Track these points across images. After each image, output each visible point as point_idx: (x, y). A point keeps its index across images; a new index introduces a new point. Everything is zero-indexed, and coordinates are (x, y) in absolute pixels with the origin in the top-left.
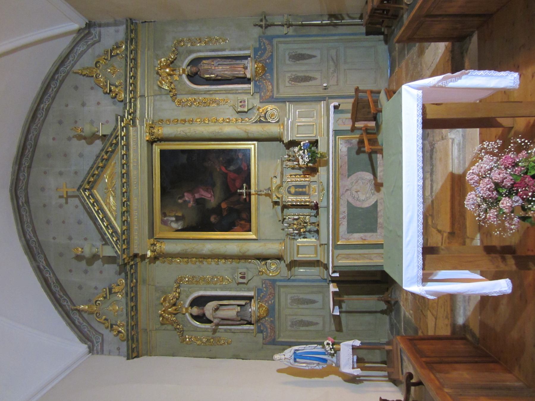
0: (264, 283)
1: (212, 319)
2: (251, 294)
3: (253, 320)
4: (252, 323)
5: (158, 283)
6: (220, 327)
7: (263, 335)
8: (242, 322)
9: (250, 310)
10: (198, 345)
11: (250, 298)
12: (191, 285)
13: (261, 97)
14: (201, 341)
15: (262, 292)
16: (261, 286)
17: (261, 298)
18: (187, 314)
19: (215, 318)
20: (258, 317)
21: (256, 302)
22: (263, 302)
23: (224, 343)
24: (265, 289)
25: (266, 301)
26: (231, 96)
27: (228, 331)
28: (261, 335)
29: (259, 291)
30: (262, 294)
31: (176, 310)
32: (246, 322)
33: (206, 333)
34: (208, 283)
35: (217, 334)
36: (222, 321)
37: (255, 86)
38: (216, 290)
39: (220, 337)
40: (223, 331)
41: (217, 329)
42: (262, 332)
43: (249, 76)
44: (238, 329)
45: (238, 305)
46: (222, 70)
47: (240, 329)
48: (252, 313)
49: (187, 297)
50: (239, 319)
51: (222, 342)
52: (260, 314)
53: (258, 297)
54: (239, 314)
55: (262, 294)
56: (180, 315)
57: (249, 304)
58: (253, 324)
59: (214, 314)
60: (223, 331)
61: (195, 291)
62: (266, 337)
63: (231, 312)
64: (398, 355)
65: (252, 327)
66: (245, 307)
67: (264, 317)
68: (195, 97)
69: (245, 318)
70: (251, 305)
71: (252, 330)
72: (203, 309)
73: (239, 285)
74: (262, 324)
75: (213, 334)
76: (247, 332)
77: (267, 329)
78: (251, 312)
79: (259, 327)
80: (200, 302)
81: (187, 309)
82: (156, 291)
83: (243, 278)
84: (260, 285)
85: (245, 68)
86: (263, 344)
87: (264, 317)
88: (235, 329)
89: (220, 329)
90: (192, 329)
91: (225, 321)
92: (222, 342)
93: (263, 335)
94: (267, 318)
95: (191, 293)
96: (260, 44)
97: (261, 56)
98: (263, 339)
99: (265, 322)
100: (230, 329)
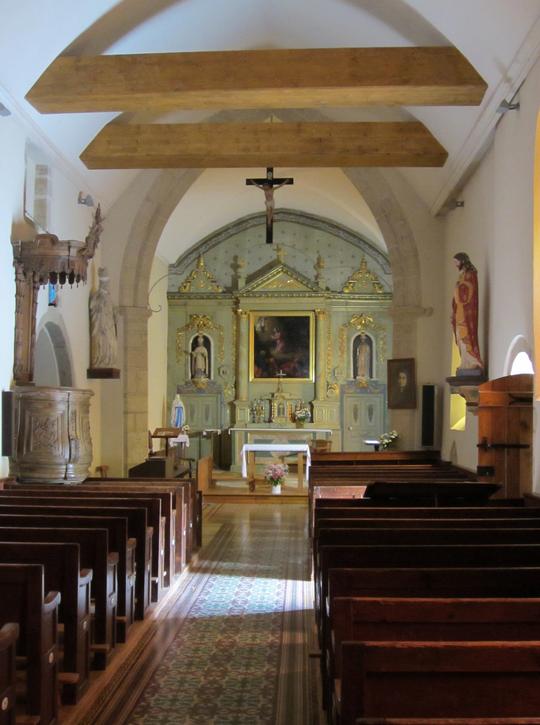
2: (212, 377)
3: (196, 380)
11: (209, 377)
13: (344, 385)
26: (346, 365)
29: (214, 383)
35: (184, 354)
37: (352, 382)
43: (358, 377)
45: (205, 370)
46: (363, 359)
49: (210, 334)
63: (201, 364)
67: (196, 386)
68: (345, 340)
76: (186, 374)
85: (363, 375)
91: (194, 361)
96: (380, 385)
97: (372, 385)
100: (188, 363)
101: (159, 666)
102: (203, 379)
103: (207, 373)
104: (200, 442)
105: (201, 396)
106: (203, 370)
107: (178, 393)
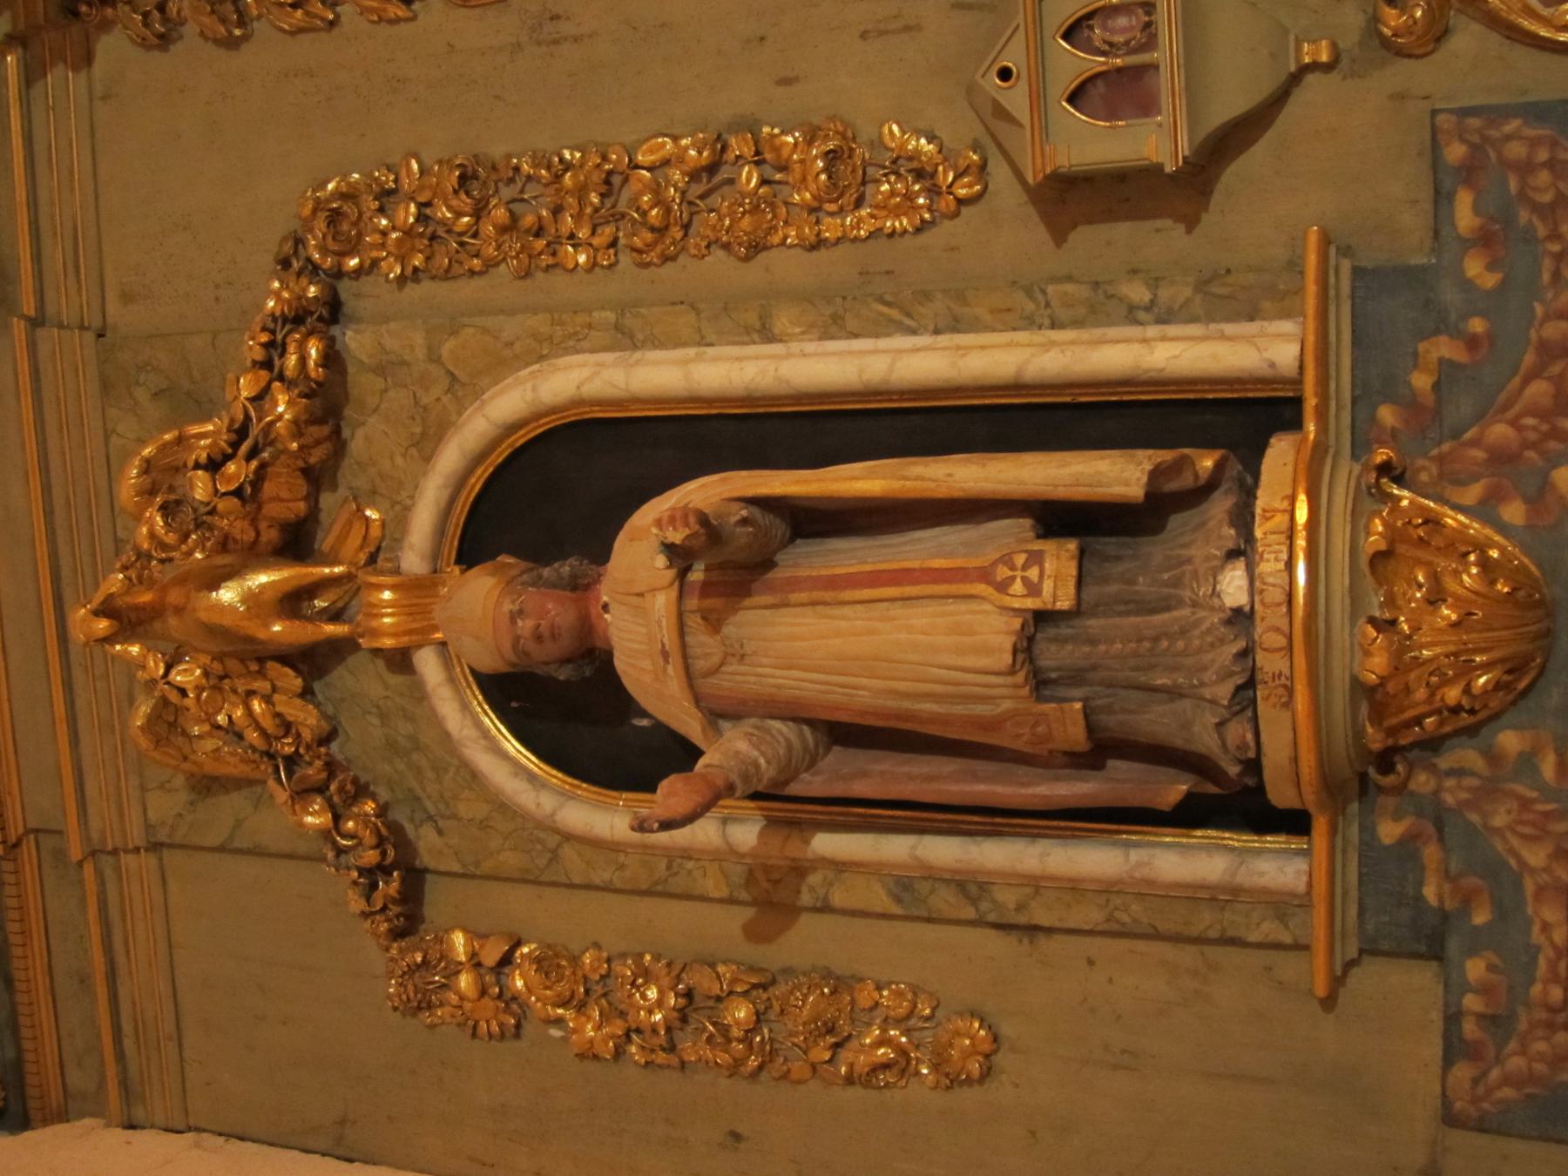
0: (1468, 173)
1: (690, 725)
2: (1265, 348)
3: (1286, 747)
4: (1280, 795)
5: (127, 297)
6: (827, 844)
7: (1453, 987)
8: (1120, 782)
9: (1233, 586)
10: (588, 1055)
11: (1245, 419)
12: (467, 290)
14: (615, 1012)
15: (1442, 325)
16: (1414, 222)
17: (1425, 419)
18: (428, 663)
19: (718, 713)
20: (1373, 698)
21: (1344, 476)
22: (1450, 477)
23: (902, 1065)
24: (1474, 267)
25: (1501, 458)
27: (945, 900)
28: (1413, 985)
29: (1380, 298)
30: (1444, 348)
31: (293, 602)
32: (1174, 789)
33: (674, 922)
34: (669, 237)
35: (808, 942)
36: (837, 758)
38: (767, 334)
39: (841, 984)
40: (878, 897)
41: (799, 870)
42: (1430, 940)
44: (1074, 888)
45: (1056, 518)
47: (1108, 889)
48: (1267, 634)
49: (426, 444)
50: (1067, 723)
51: (872, 1045)
52: (1401, 663)
53: (1363, 398)
54: (1053, 655)
55: (1444, 348)
56: (360, 680)
57: (1220, 505)
58: (1295, 823)
59: (704, 644)
60: (878, 897)
61: (503, 362)
62: (1495, 1022)
63: (918, 628)
64: (905, 818)
65: (1276, 865)
66: (1155, 549)
67: (1473, 722)
69: (1156, 721)
70: (1243, 518)
71: (1280, 904)
72: (581, 587)
73: (1086, 238)
74: (1439, 818)
75: (754, 933)
76: (1201, 927)
77: (1508, 910)
78: (1241, 618)
79: (1385, 872)
80: (554, 494)
81: (418, 590)
82: (106, 386)
83: (1118, 91)
84: (1395, 208)
86: (1450, 1119)
87: (1473, 722)
88: (1036, 883)
89: (840, 867)
90: (511, 860)
91: (864, 754)
92: (872, 1045)
93: (1453, 987)
94: (1509, 741)
95: (465, 388)
98: (1454, 1049)
99: (1489, 791)
100: (969, 885)
101: (1189, 560)
102: (1280, 555)
103: (1118, 474)
104: (1279, 605)
105: (890, 546)
106: (1054, 573)
107: (1527, 500)
